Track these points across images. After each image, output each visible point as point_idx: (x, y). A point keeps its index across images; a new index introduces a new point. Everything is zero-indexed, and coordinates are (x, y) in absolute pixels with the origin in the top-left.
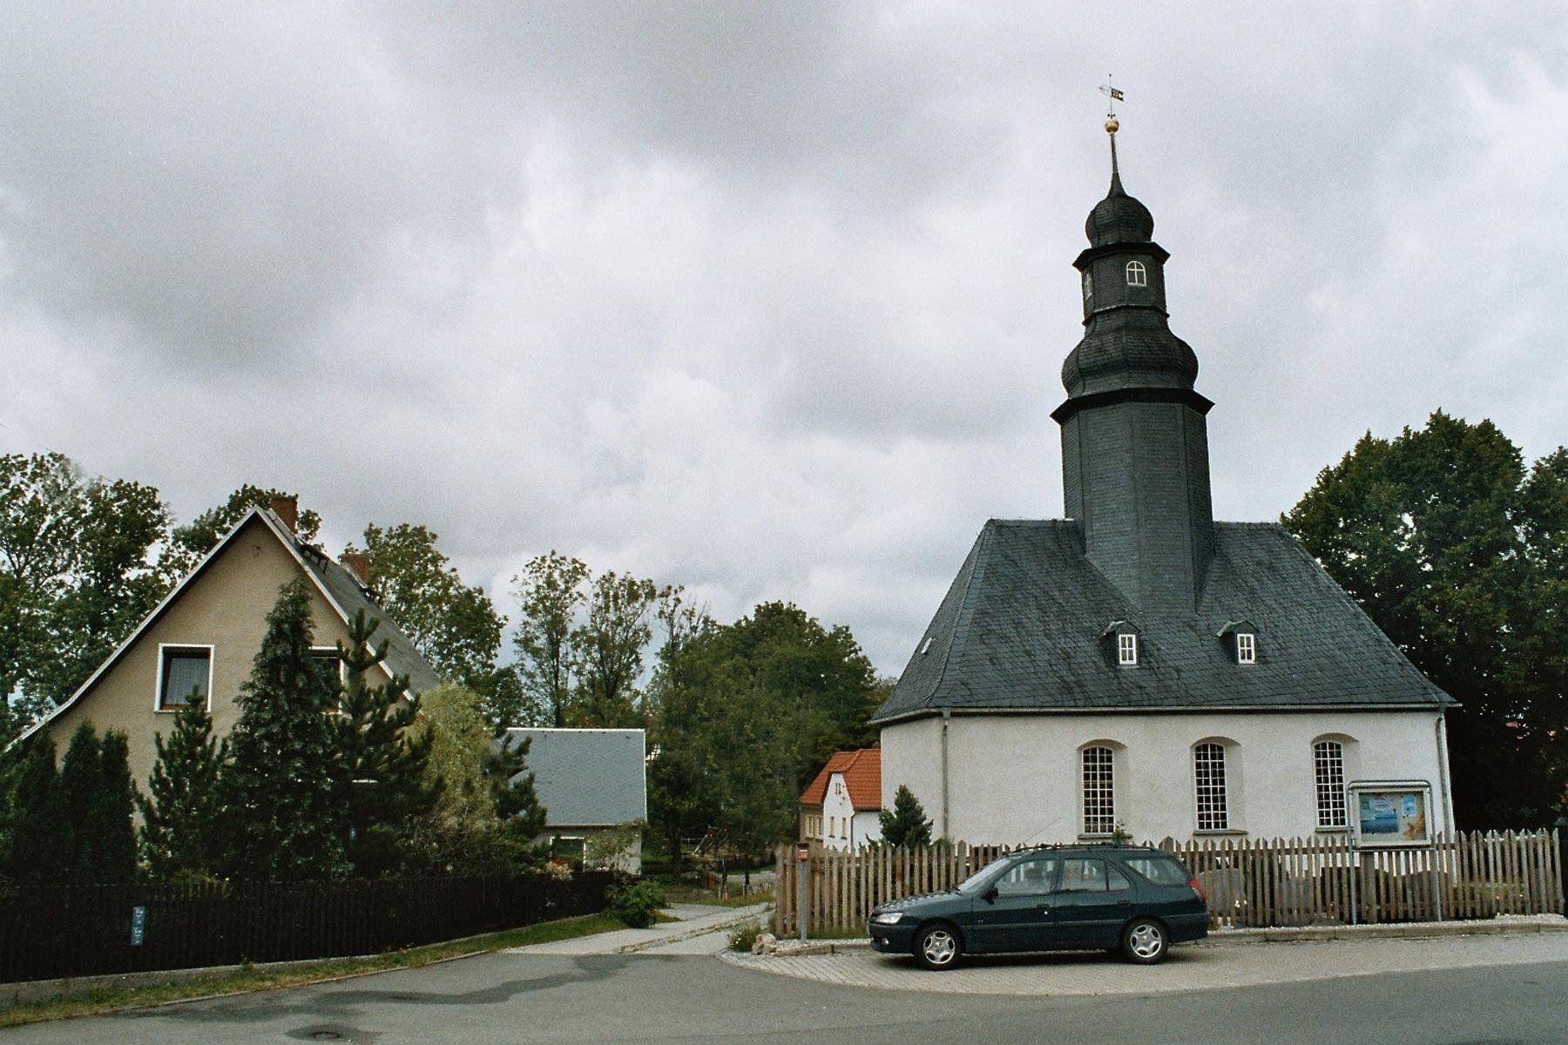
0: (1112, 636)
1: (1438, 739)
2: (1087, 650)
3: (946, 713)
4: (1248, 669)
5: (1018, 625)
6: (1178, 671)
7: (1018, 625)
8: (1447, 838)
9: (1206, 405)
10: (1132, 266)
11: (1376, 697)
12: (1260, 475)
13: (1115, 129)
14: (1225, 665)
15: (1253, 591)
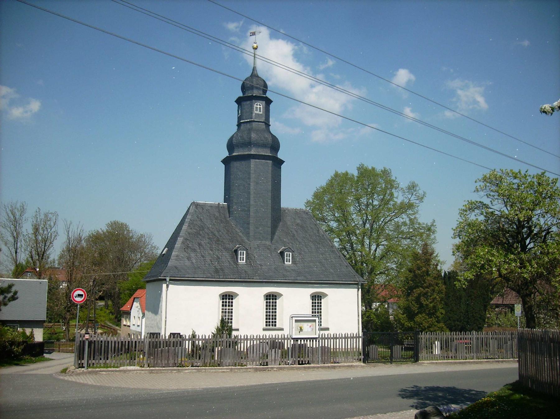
0: (236, 251)
1: (358, 295)
2: (226, 257)
3: (168, 279)
4: (289, 266)
5: (200, 244)
6: (261, 265)
7: (200, 244)
8: (359, 334)
9: (282, 162)
10: (257, 105)
11: (336, 279)
12: (296, 194)
13: (256, 49)
14: (280, 264)
15: (294, 236)
